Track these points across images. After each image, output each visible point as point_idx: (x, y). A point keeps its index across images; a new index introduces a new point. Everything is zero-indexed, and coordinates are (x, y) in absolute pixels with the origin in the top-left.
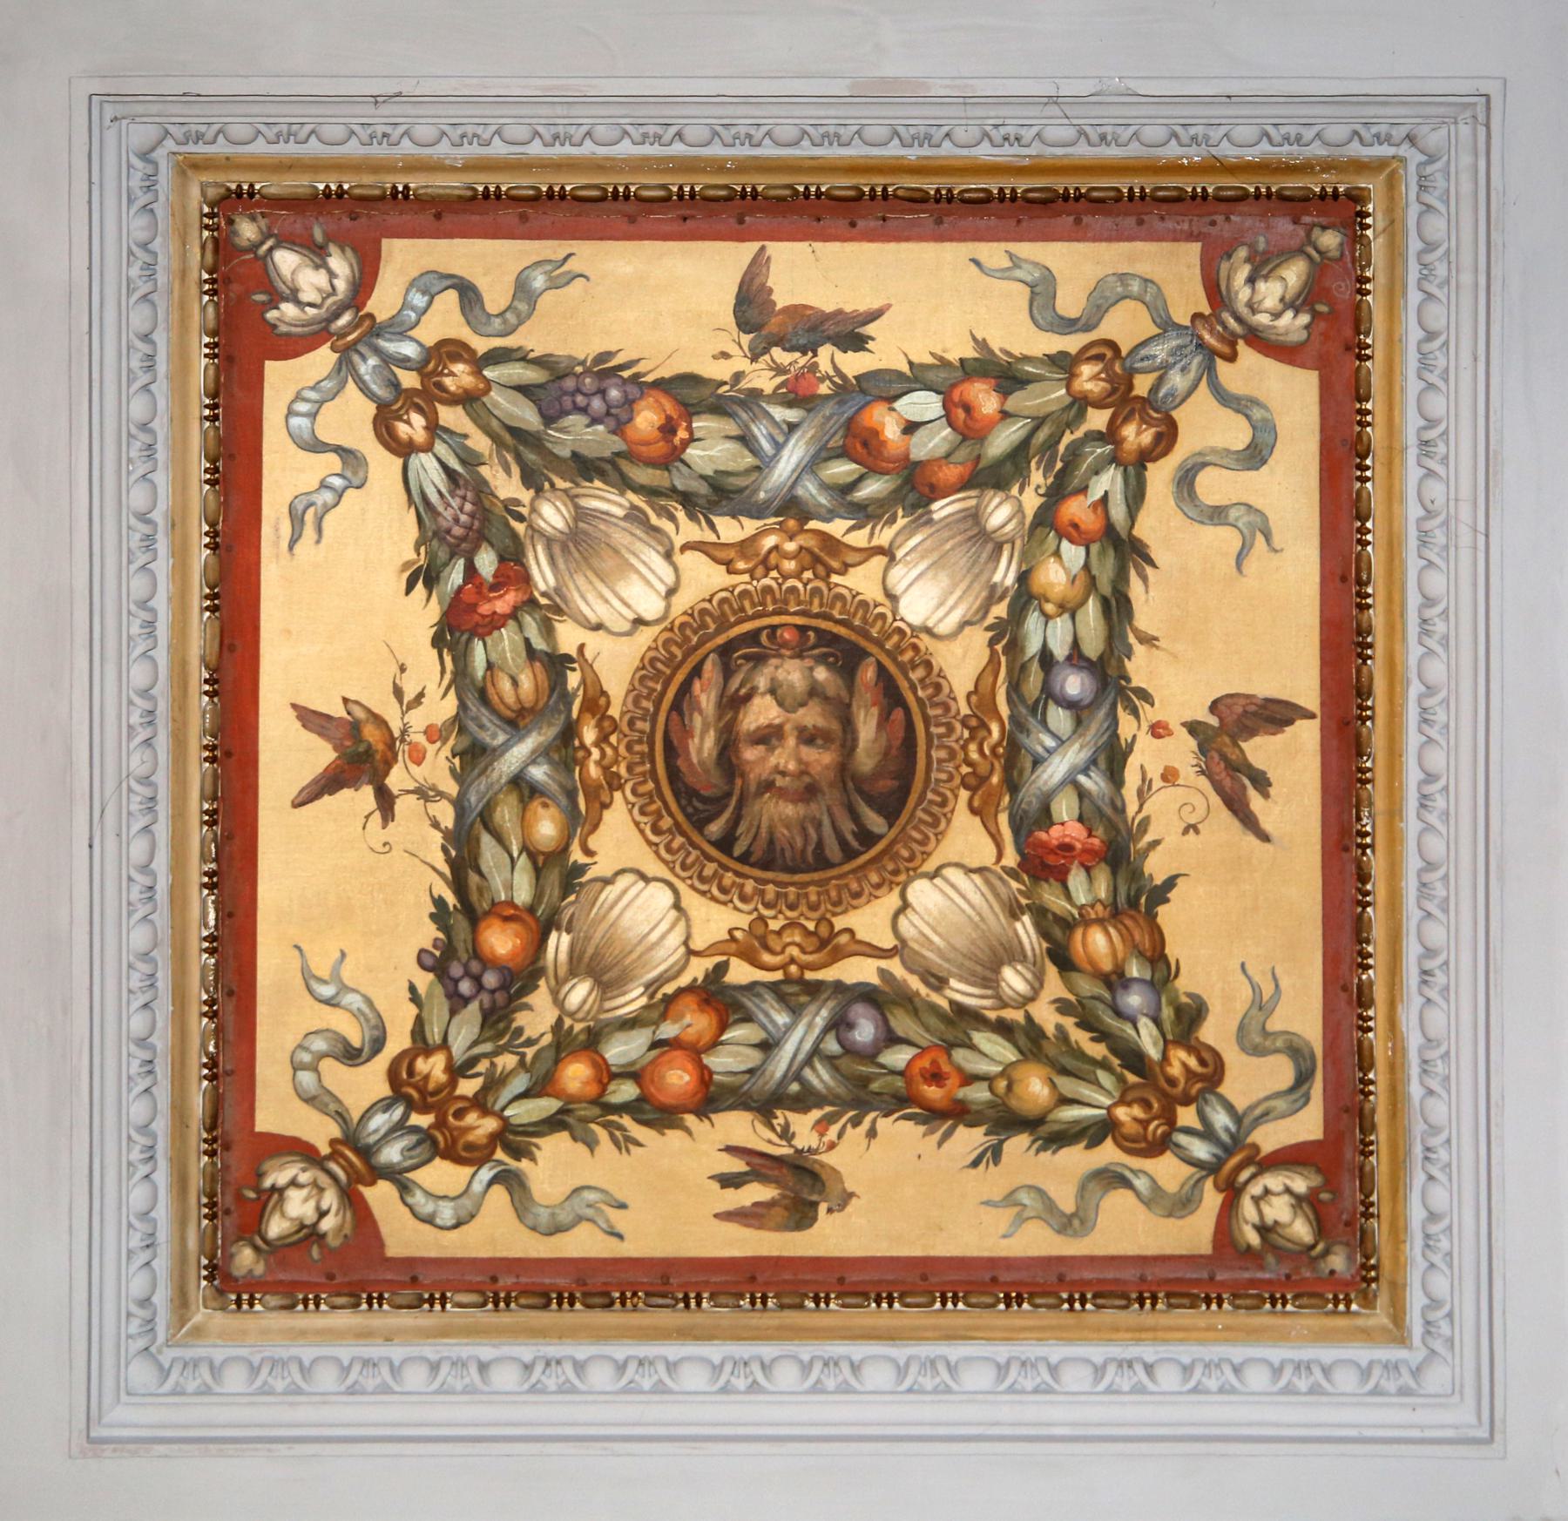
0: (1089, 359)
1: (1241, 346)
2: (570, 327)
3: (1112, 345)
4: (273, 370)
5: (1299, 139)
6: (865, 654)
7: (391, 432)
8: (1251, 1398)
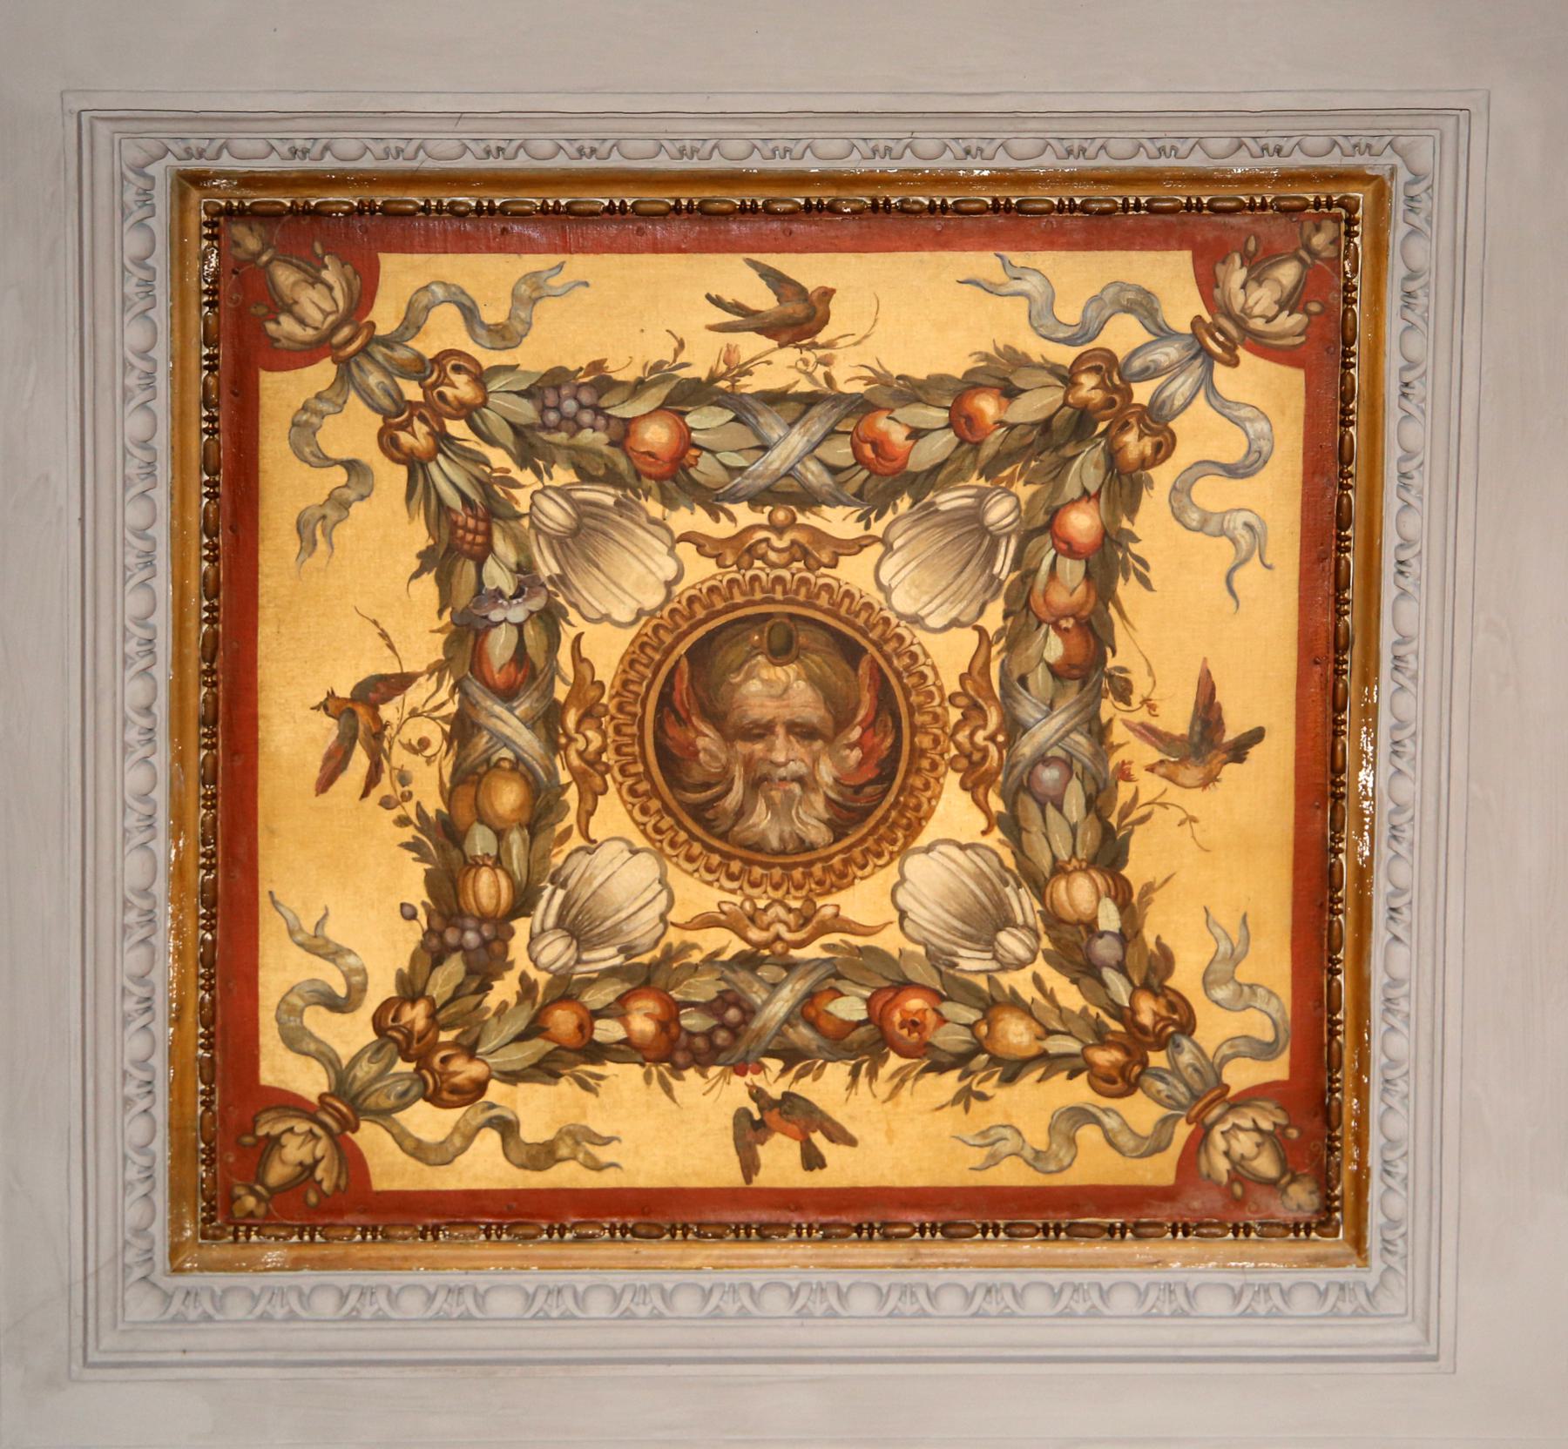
0: (1089, 370)
1: (1241, 352)
2: (561, 339)
3: (1110, 357)
4: (269, 381)
5: (1278, 151)
6: (865, 651)
7: (395, 442)
8: (854, 1322)
